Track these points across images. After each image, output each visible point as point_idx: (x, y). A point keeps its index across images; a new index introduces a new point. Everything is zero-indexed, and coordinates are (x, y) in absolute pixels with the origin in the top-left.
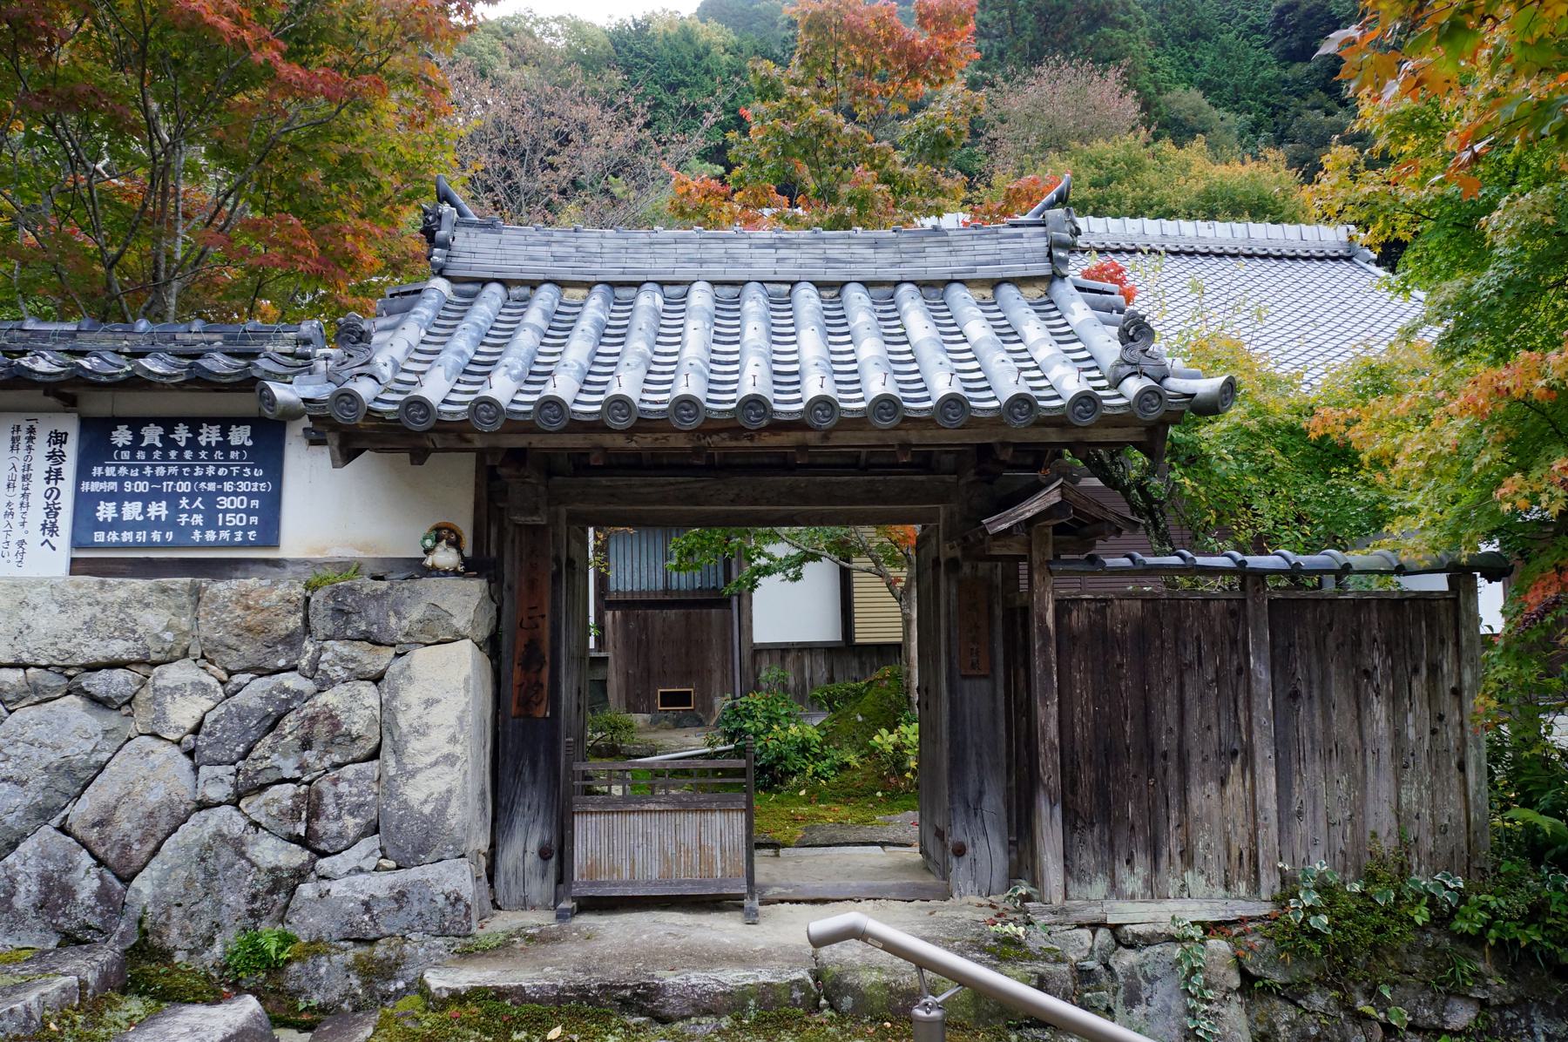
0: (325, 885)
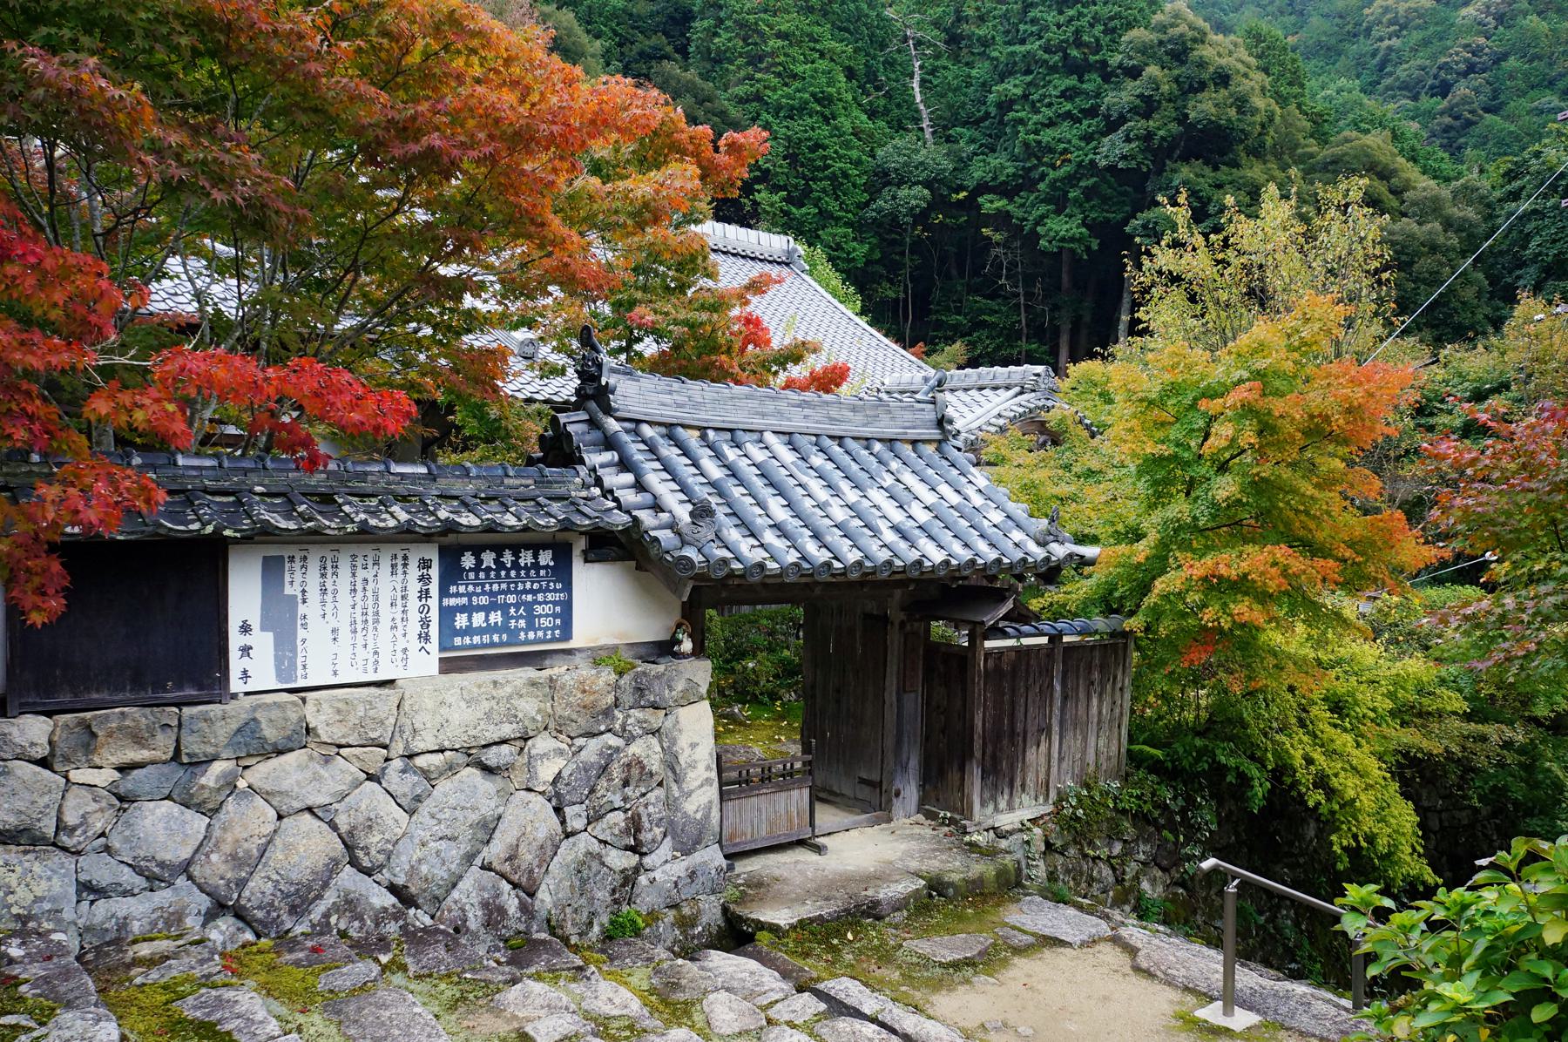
0: (651, 875)
